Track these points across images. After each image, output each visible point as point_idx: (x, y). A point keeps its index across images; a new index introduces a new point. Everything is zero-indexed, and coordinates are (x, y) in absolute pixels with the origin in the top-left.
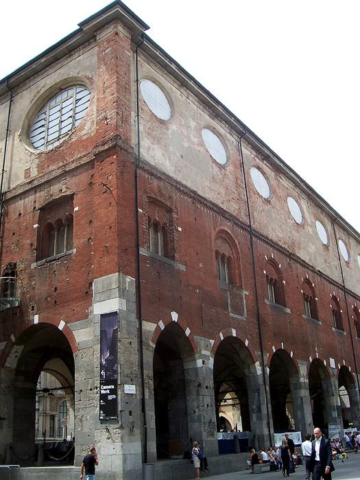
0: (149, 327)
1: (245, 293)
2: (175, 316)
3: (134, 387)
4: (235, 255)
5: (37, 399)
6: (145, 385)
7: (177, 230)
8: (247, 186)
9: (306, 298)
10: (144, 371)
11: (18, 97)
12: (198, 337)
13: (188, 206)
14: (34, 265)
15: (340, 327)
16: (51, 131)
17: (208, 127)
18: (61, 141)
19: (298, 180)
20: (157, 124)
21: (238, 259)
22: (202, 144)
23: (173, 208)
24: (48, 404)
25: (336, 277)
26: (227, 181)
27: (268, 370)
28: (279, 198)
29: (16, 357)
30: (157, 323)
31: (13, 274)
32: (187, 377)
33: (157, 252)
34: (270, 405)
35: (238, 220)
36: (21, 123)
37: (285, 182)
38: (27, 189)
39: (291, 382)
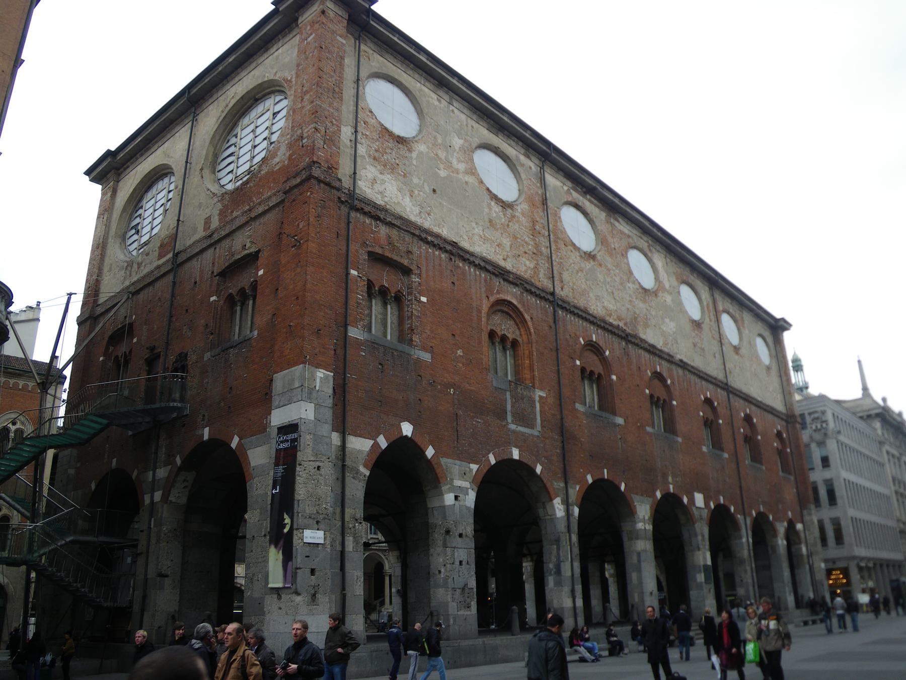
0: (360, 445)
2: (407, 429)
3: (321, 534)
4: (525, 337)
6: (347, 531)
7: (420, 301)
8: (552, 236)
10: (347, 510)
11: (202, 114)
12: (449, 460)
13: (440, 265)
14: (207, 355)
15: (717, 445)
16: (241, 161)
20: (391, 144)
21: (530, 342)
22: (472, 171)
23: (413, 267)
25: (713, 368)
27: (576, 511)
28: (611, 252)
29: (185, 487)
30: (374, 437)
32: (432, 520)
35: (532, 285)
36: (204, 152)
37: (624, 227)
38: (204, 246)
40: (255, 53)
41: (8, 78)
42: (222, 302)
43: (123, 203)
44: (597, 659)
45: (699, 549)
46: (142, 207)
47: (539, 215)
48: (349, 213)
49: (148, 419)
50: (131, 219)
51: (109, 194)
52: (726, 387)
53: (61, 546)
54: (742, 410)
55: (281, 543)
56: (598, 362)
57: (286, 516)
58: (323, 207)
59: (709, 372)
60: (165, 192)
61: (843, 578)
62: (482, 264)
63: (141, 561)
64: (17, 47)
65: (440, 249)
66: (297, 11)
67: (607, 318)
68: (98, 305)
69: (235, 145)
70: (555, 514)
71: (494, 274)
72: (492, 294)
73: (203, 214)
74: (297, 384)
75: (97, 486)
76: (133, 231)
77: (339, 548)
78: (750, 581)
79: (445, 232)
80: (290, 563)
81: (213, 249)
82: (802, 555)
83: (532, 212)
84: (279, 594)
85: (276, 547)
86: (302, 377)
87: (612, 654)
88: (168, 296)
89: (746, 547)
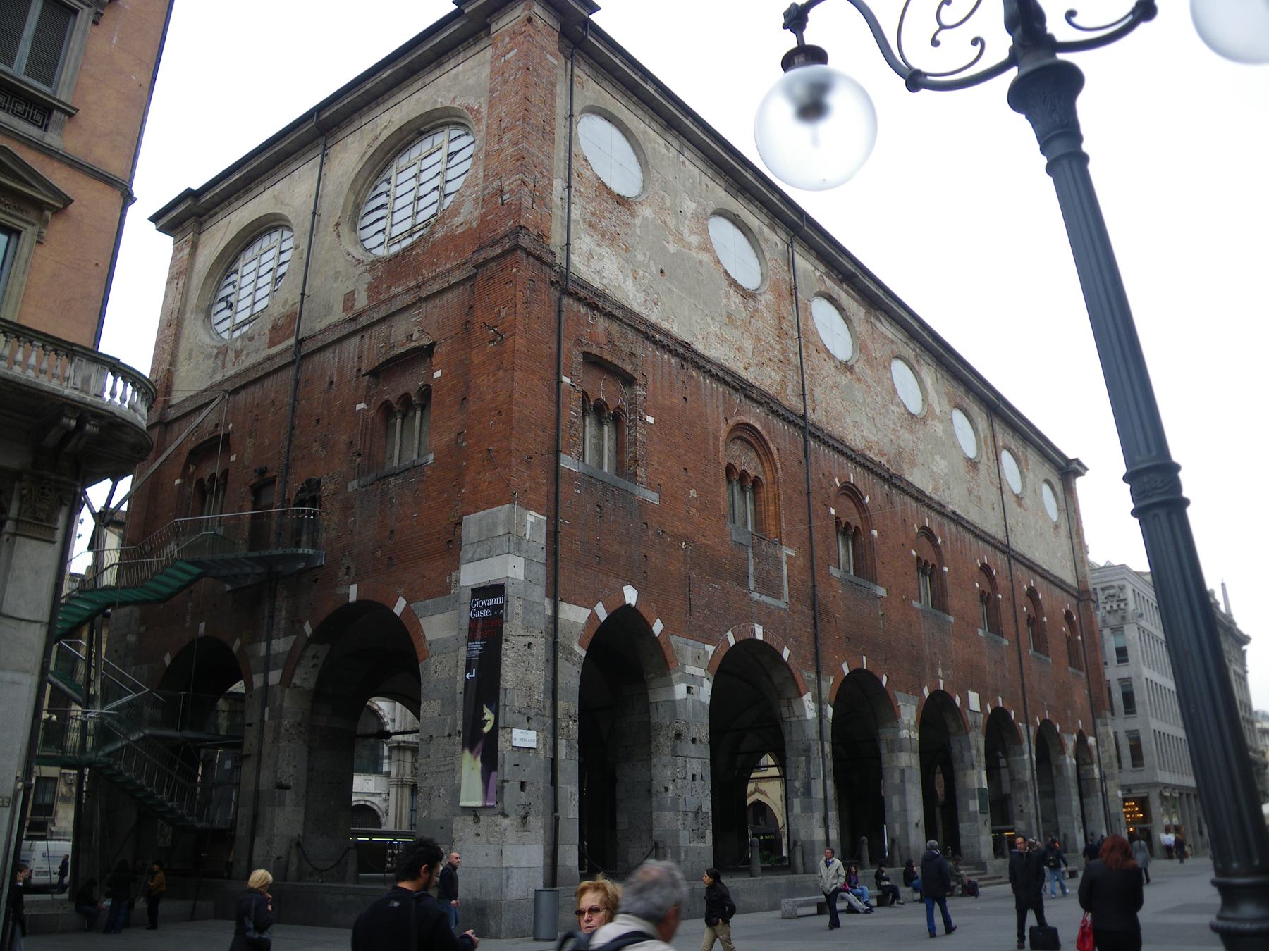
0: (575, 615)
1: (787, 551)
2: (631, 595)
3: (532, 735)
5: (386, 753)
6: (560, 731)
7: (645, 422)
8: (803, 334)
9: (923, 567)
10: (560, 703)
12: (681, 639)
13: (670, 374)
14: (353, 486)
15: (995, 627)
17: (722, 213)
18: (416, 236)
19: (916, 325)
20: (610, 205)
22: (707, 247)
23: (638, 375)
24: (408, 766)
25: (992, 526)
26: (760, 324)
27: (830, 711)
28: (871, 362)
30: (591, 606)
31: (314, 501)
32: (655, 719)
33: (600, 465)
34: (830, 783)
35: (780, 404)
36: (341, 201)
37: (887, 329)
38: (346, 331)
39: (882, 737)
40: (422, 68)
41: (146, 94)
42: (373, 412)
43: (209, 264)
44: (870, 910)
45: (973, 767)
46: (236, 272)
47: (787, 309)
48: (560, 299)
49: (259, 570)
50: (218, 288)
51: (186, 251)
52: (1006, 549)
53: (136, 742)
54: (1026, 580)
55: (480, 746)
56: (855, 511)
57: (486, 710)
58: (533, 290)
59: (986, 530)
60: (273, 253)
61: (1139, 812)
62: (721, 374)
63: (248, 768)
64: (156, 51)
65: (670, 351)
66: (489, 16)
67: (867, 452)
68: (170, 407)
69: (387, 193)
70: (805, 715)
71: (733, 388)
72: (732, 416)
73: (342, 288)
74: (501, 531)
75: (173, 661)
76: (224, 304)
77: (550, 755)
78: (1033, 811)
79: (675, 329)
80: (493, 774)
81: (358, 338)
82: (1094, 779)
83: (779, 305)
84: (476, 816)
85: (471, 751)
86: (509, 522)
87: (882, 902)
88: (288, 399)
89: (1028, 766)
